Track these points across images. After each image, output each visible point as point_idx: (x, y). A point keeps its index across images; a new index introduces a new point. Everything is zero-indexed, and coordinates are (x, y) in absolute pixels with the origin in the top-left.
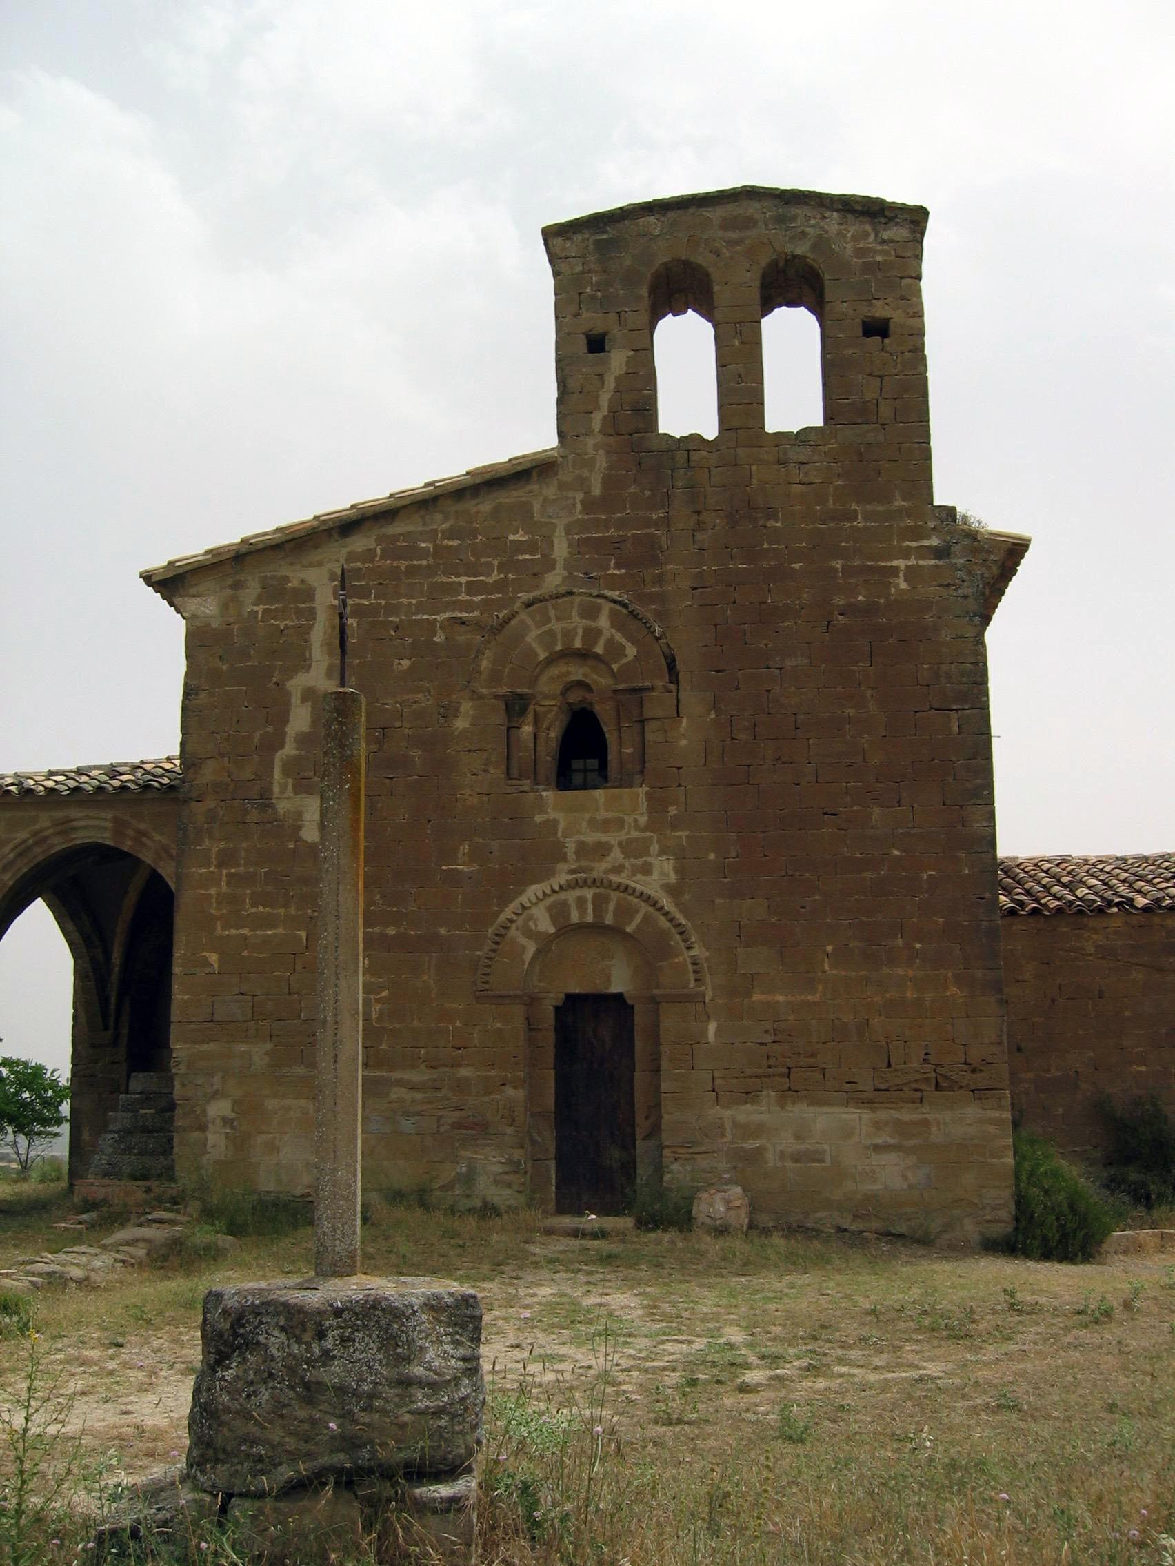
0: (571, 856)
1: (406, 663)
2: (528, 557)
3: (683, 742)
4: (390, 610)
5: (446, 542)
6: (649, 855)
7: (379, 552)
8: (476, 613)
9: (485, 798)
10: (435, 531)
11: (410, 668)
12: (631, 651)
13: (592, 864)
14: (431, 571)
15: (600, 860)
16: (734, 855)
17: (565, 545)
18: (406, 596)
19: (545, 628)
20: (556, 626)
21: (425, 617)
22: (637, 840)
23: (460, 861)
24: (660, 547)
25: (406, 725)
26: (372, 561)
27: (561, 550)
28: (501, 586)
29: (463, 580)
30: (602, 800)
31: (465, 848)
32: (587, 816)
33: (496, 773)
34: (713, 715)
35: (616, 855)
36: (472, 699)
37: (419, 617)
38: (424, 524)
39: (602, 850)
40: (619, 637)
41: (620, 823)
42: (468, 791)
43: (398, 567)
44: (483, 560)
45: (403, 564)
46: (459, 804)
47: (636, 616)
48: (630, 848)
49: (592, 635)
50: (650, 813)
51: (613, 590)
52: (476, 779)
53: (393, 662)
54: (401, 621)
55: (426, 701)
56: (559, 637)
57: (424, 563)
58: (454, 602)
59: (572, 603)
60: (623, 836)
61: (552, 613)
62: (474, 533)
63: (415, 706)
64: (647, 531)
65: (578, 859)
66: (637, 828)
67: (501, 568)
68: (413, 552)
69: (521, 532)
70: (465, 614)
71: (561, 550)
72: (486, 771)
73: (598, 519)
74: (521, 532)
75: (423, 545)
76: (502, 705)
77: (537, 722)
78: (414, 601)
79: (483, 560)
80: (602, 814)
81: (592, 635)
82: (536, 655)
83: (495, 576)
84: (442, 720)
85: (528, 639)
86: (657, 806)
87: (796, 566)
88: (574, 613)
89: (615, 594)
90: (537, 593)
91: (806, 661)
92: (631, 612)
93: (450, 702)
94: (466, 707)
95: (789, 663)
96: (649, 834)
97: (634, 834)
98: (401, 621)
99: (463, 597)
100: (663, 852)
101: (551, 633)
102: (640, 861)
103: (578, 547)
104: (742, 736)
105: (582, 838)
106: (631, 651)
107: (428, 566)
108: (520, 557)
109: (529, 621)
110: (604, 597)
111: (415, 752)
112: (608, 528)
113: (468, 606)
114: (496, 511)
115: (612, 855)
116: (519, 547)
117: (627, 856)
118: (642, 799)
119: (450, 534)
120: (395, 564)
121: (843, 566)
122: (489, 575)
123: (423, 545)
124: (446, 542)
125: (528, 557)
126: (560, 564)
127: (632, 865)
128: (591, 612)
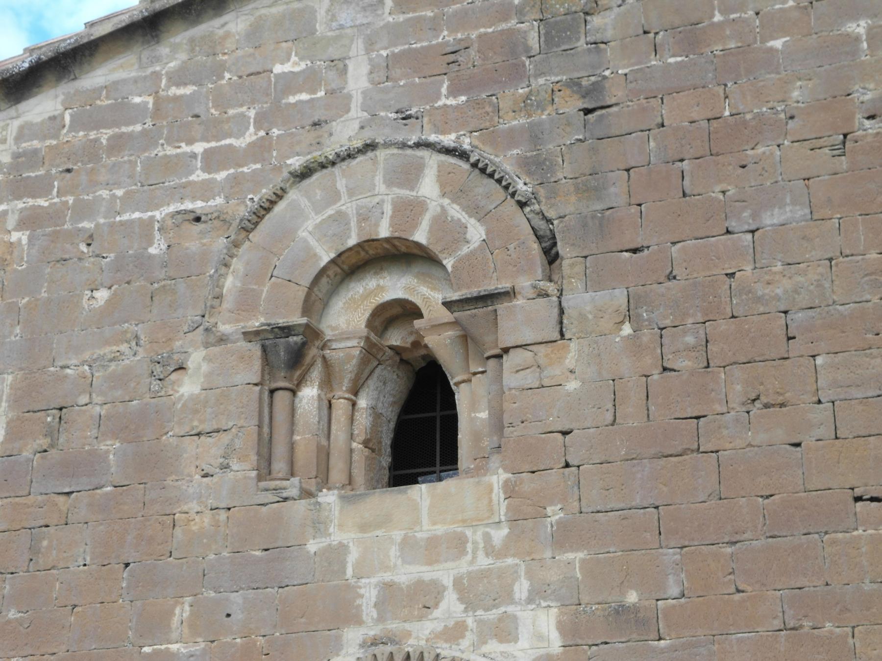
0: (369, 612)
1: (102, 295)
2: (304, 97)
3: (572, 385)
4: (83, 210)
5: (174, 91)
6: (510, 599)
7: (67, 118)
8: (219, 201)
9: (223, 515)
10: (157, 75)
11: (108, 301)
12: (476, 232)
13: (407, 626)
14: (149, 139)
15: (420, 618)
16: (675, 591)
17: (365, 69)
18: (108, 185)
19: (330, 211)
20: (348, 206)
21: (137, 215)
22: (484, 574)
23: (174, 635)
24: (527, 49)
25: (97, 399)
26: (56, 136)
27: (358, 79)
28: (258, 150)
29: (199, 148)
30: (425, 504)
31: (183, 611)
32: (398, 535)
33: (243, 469)
34: (627, 330)
35: (450, 606)
36: (207, 345)
37: (126, 217)
38: (142, 67)
39: (424, 597)
40: (456, 212)
41: (458, 544)
42: (194, 506)
43: (96, 140)
44: (231, 112)
45: (105, 135)
46: (178, 531)
47: (483, 171)
48: (470, 592)
49: (409, 210)
50: (513, 521)
51: (444, 133)
52: (209, 481)
53: (81, 296)
54: (97, 225)
55: (135, 359)
56: (353, 224)
57: (138, 128)
58: (184, 186)
59: (374, 161)
60: (463, 566)
61: (341, 184)
62: (218, 71)
63: (113, 366)
64: (504, 26)
65: (381, 619)
66: (490, 550)
67: (259, 122)
68: (122, 112)
69: (294, 58)
70: (199, 204)
71: (358, 79)
72: (225, 467)
73: (419, 19)
74: (294, 58)
75: (137, 100)
76: (255, 349)
77: (327, 383)
78: (119, 193)
79: (231, 112)
80: (427, 529)
81: (409, 210)
82: (320, 258)
83: (251, 135)
84: (155, 385)
85: (302, 234)
86: (524, 512)
87: (777, 44)
88: (379, 179)
89: (448, 140)
90: (317, 155)
91: (802, 212)
92: (475, 165)
93: (172, 352)
94: (196, 359)
95: (771, 219)
96: (510, 561)
97: (484, 562)
98: (97, 225)
99: (199, 176)
100: (536, 595)
101: (340, 217)
102: (493, 615)
103: (385, 71)
104: (683, 363)
105: (387, 577)
106: (476, 232)
107: (144, 133)
108: (292, 99)
109: (304, 202)
110: (428, 145)
111: (111, 447)
112: (435, 29)
113: (205, 190)
114: (254, 34)
115: (443, 605)
116: (290, 83)
117: (470, 605)
118: (498, 494)
119: (177, 79)
120: (93, 135)
121: (869, 29)
122: (240, 134)
123: (137, 100)
124: (174, 91)
125: (304, 97)
126: (357, 101)
127: (480, 622)
128: (409, 176)
